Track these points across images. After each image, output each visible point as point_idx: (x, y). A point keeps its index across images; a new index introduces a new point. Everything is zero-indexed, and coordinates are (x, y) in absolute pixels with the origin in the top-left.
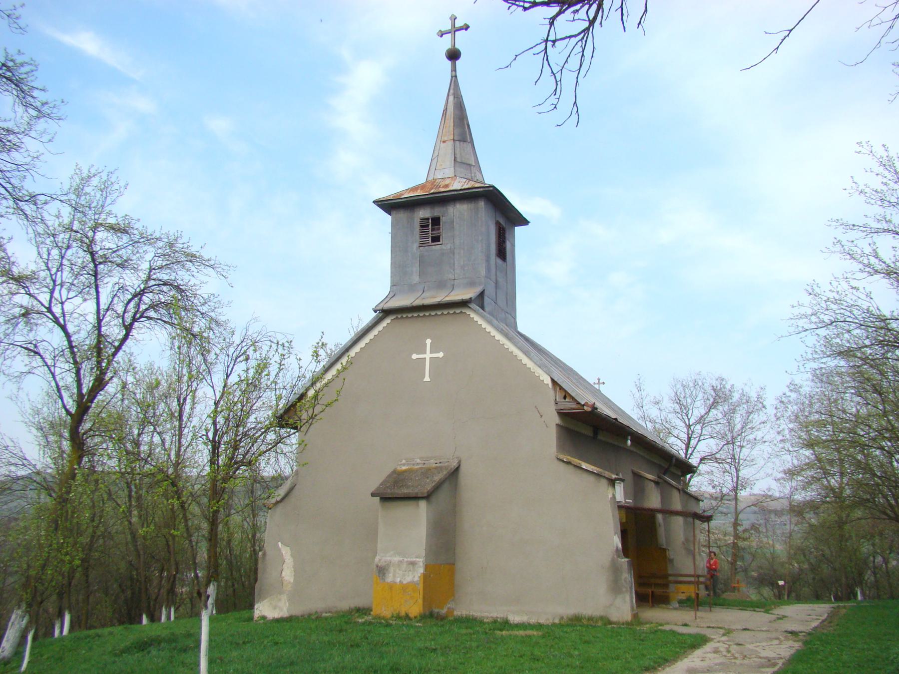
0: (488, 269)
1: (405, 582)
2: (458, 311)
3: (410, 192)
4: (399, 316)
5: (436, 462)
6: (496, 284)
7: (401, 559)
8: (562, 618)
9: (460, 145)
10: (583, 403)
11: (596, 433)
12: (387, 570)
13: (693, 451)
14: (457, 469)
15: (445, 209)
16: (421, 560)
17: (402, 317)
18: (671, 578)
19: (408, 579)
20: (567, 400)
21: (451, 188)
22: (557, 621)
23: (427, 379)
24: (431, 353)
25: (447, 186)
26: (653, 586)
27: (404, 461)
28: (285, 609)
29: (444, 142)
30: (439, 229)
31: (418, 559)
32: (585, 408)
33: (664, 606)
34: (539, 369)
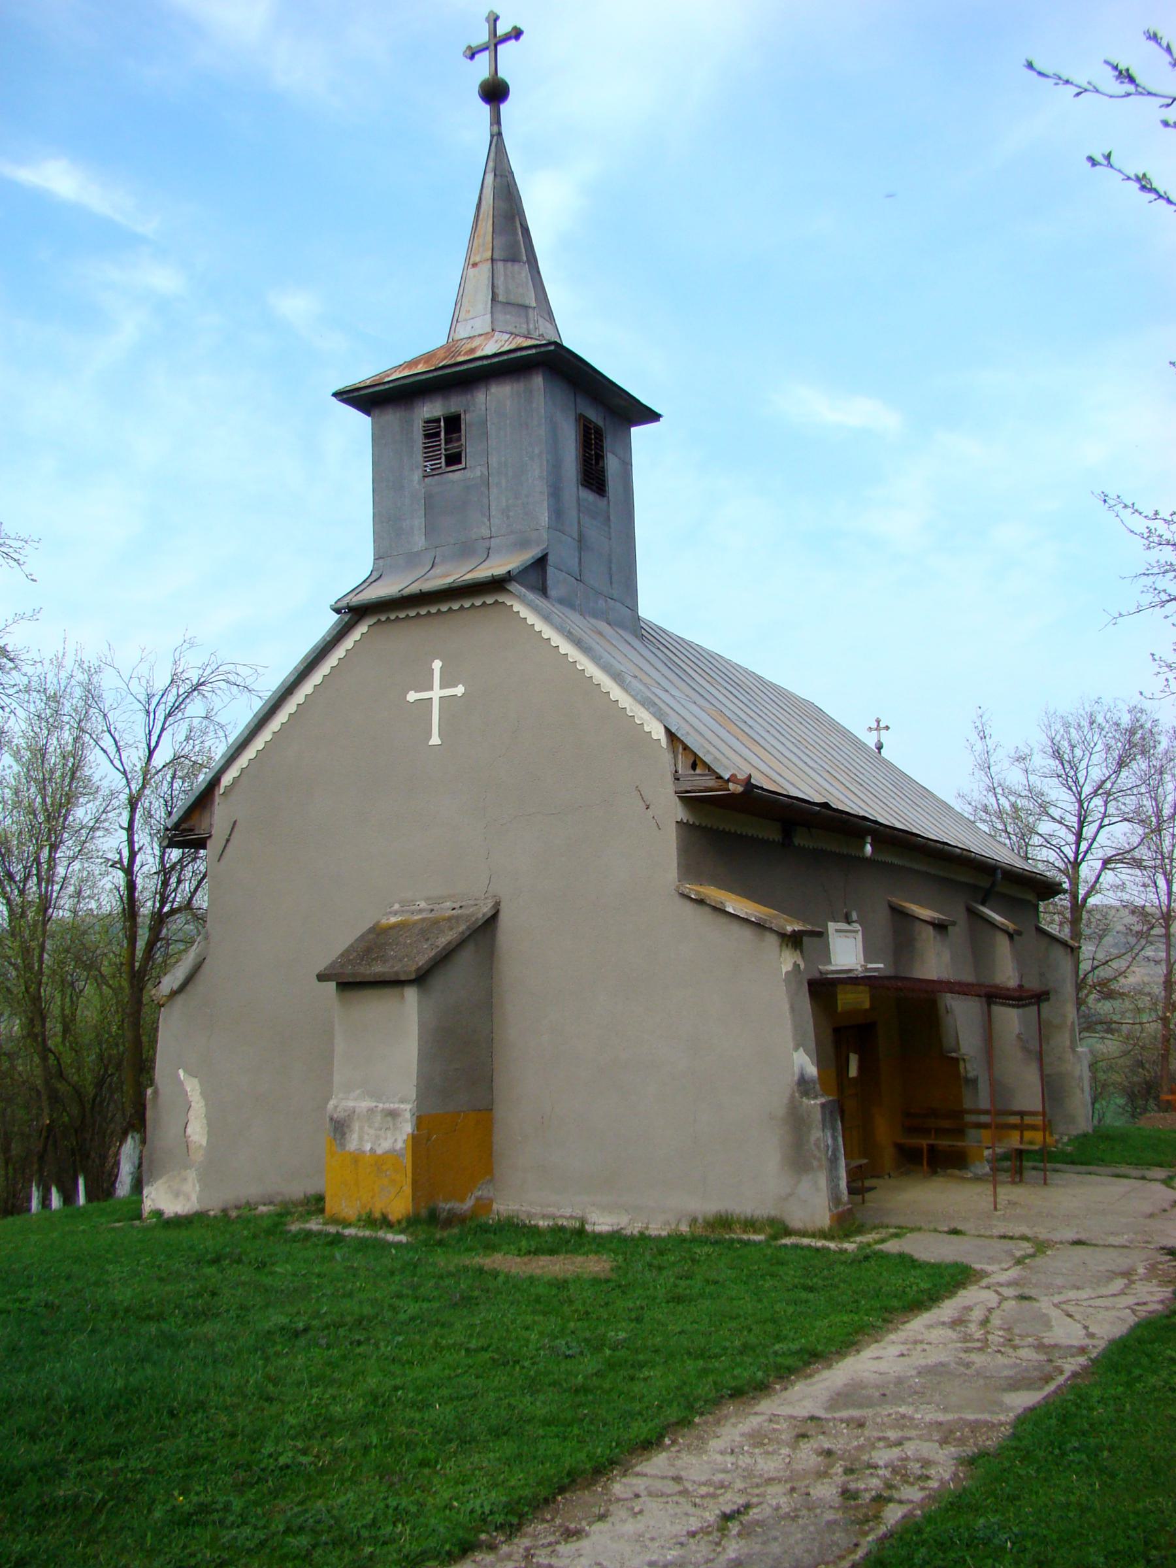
0: (557, 513)
1: (379, 1151)
2: (490, 601)
3: (403, 369)
4: (383, 618)
5: (454, 905)
6: (580, 541)
7: (374, 1104)
8: (694, 1221)
9: (505, 269)
10: (726, 777)
11: (787, 833)
12: (349, 1127)
13: (1089, 848)
14: (492, 920)
15: (469, 397)
16: (409, 1107)
17: (388, 618)
18: (969, 1118)
19: (385, 1145)
20: (698, 771)
21: (479, 354)
22: (684, 1228)
23: (435, 740)
24: (442, 687)
25: (473, 350)
26: (933, 1132)
27: (396, 907)
28: (194, 1197)
29: (475, 265)
30: (459, 439)
31: (402, 1106)
32: (731, 786)
33: (957, 1172)
34: (643, 710)
